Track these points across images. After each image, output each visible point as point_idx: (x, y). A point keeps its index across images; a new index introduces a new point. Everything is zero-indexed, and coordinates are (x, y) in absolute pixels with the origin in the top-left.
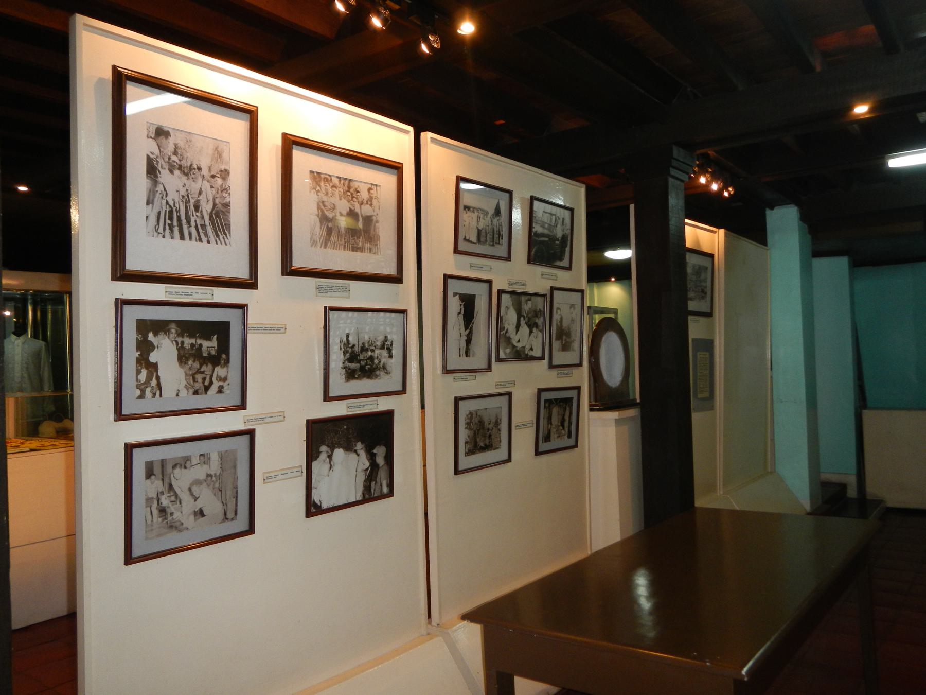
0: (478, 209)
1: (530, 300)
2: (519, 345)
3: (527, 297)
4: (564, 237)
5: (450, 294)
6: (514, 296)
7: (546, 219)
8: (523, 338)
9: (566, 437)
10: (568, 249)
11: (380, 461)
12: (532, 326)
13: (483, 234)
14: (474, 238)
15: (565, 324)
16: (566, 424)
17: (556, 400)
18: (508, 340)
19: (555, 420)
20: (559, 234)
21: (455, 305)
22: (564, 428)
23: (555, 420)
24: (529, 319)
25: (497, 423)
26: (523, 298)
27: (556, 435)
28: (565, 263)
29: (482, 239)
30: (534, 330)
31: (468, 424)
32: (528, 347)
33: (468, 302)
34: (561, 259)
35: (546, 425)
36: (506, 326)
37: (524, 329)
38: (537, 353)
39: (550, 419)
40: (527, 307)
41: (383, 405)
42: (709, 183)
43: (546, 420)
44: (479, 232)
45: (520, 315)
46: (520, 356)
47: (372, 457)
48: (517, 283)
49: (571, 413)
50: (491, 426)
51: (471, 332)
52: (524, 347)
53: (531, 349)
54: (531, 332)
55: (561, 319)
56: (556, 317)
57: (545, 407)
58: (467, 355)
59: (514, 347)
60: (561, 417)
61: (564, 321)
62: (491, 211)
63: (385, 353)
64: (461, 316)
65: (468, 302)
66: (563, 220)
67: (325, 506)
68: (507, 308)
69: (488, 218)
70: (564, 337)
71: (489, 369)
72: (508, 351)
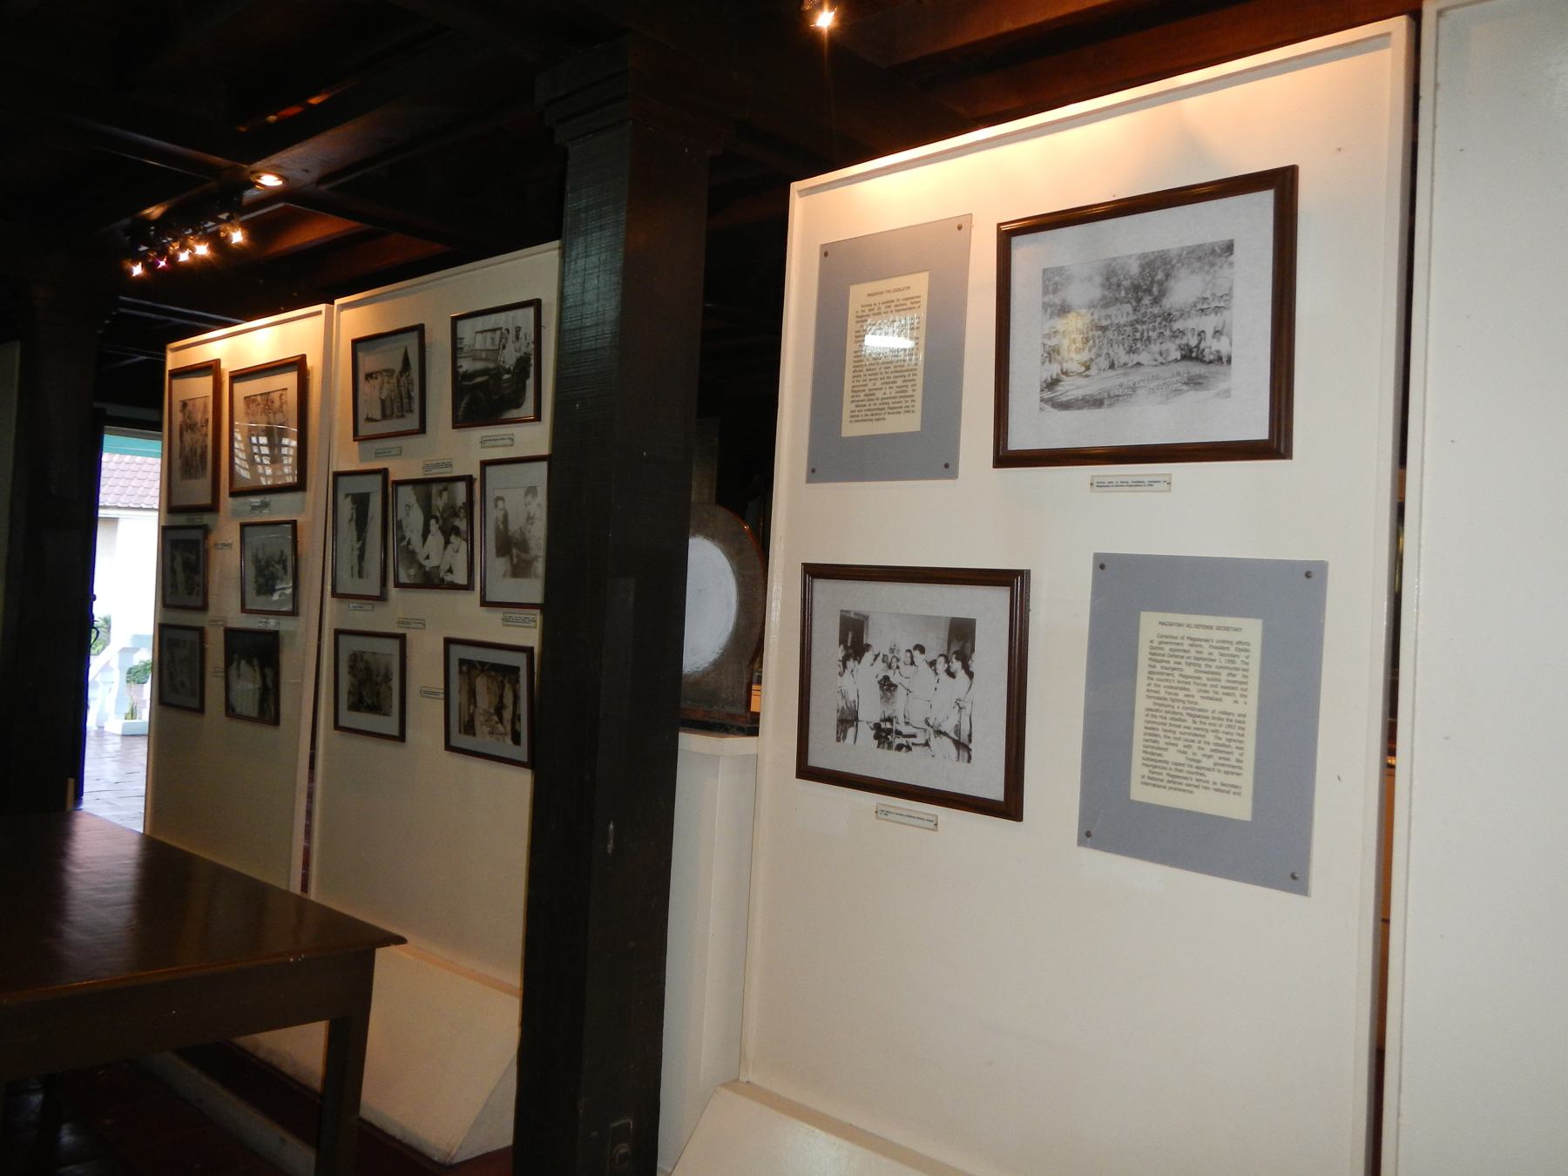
0: (380, 372)
1: (445, 489)
2: (429, 564)
3: (440, 487)
4: (523, 362)
5: (341, 496)
6: (421, 488)
7: (480, 343)
8: (433, 552)
9: (508, 740)
10: (530, 383)
11: (269, 681)
12: (449, 532)
13: (388, 404)
14: (377, 414)
15: (513, 527)
16: (507, 714)
17: (483, 664)
18: (411, 556)
19: (484, 701)
20: (509, 358)
21: (346, 509)
22: (501, 721)
23: (484, 701)
24: (445, 521)
25: (387, 678)
26: (435, 489)
27: (486, 729)
28: (528, 408)
29: (388, 412)
30: (453, 538)
31: (352, 668)
32: (445, 567)
33: (361, 502)
34: (518, 404)
35: (465, 701)
36: (408, 535)
37: (436, 538)
38: (460, 577)
39: (472, 694)
40: (439, 503)
41: (271, 623)
42: (219, 244)
43: (465, 695)
44: (383, 401)
45: (428, 515)
46: (431, 581)
47: (264, 676)
48: (438, 466)
49: (516, 698)
50: (379, 679)
51: (363, 545)
52: (438, 567)
53: (450, 571)
54: (447, 542)
55: (506, 516)
56: (494, 515)
57: (461, 672)
58: (360, 576)
59: (421, 566)
60: (495, 701)
61: (511, 518)
62: (398, 366)
63: (279, 567)
64: (353, 524)
65: (361, 502)
66: (518, 329)
67: (238, 710)
68: (408, 506)
69: (394, 380)
70: (515, 551)
71: (382, 598)
72: (412, 572)
